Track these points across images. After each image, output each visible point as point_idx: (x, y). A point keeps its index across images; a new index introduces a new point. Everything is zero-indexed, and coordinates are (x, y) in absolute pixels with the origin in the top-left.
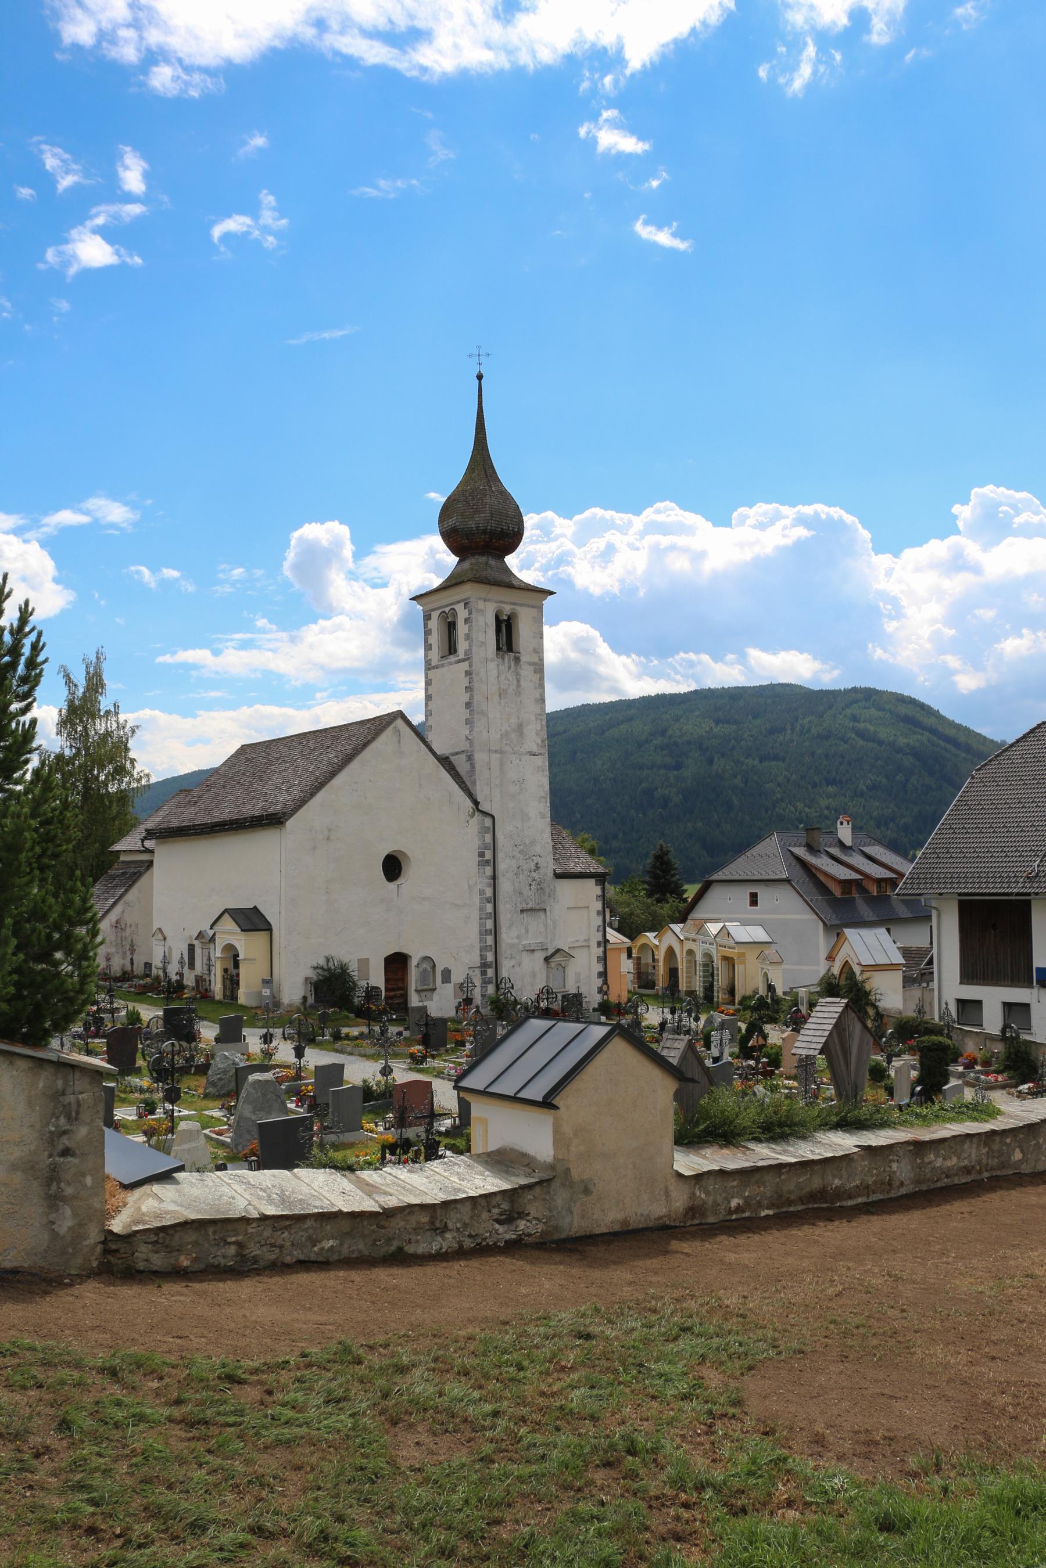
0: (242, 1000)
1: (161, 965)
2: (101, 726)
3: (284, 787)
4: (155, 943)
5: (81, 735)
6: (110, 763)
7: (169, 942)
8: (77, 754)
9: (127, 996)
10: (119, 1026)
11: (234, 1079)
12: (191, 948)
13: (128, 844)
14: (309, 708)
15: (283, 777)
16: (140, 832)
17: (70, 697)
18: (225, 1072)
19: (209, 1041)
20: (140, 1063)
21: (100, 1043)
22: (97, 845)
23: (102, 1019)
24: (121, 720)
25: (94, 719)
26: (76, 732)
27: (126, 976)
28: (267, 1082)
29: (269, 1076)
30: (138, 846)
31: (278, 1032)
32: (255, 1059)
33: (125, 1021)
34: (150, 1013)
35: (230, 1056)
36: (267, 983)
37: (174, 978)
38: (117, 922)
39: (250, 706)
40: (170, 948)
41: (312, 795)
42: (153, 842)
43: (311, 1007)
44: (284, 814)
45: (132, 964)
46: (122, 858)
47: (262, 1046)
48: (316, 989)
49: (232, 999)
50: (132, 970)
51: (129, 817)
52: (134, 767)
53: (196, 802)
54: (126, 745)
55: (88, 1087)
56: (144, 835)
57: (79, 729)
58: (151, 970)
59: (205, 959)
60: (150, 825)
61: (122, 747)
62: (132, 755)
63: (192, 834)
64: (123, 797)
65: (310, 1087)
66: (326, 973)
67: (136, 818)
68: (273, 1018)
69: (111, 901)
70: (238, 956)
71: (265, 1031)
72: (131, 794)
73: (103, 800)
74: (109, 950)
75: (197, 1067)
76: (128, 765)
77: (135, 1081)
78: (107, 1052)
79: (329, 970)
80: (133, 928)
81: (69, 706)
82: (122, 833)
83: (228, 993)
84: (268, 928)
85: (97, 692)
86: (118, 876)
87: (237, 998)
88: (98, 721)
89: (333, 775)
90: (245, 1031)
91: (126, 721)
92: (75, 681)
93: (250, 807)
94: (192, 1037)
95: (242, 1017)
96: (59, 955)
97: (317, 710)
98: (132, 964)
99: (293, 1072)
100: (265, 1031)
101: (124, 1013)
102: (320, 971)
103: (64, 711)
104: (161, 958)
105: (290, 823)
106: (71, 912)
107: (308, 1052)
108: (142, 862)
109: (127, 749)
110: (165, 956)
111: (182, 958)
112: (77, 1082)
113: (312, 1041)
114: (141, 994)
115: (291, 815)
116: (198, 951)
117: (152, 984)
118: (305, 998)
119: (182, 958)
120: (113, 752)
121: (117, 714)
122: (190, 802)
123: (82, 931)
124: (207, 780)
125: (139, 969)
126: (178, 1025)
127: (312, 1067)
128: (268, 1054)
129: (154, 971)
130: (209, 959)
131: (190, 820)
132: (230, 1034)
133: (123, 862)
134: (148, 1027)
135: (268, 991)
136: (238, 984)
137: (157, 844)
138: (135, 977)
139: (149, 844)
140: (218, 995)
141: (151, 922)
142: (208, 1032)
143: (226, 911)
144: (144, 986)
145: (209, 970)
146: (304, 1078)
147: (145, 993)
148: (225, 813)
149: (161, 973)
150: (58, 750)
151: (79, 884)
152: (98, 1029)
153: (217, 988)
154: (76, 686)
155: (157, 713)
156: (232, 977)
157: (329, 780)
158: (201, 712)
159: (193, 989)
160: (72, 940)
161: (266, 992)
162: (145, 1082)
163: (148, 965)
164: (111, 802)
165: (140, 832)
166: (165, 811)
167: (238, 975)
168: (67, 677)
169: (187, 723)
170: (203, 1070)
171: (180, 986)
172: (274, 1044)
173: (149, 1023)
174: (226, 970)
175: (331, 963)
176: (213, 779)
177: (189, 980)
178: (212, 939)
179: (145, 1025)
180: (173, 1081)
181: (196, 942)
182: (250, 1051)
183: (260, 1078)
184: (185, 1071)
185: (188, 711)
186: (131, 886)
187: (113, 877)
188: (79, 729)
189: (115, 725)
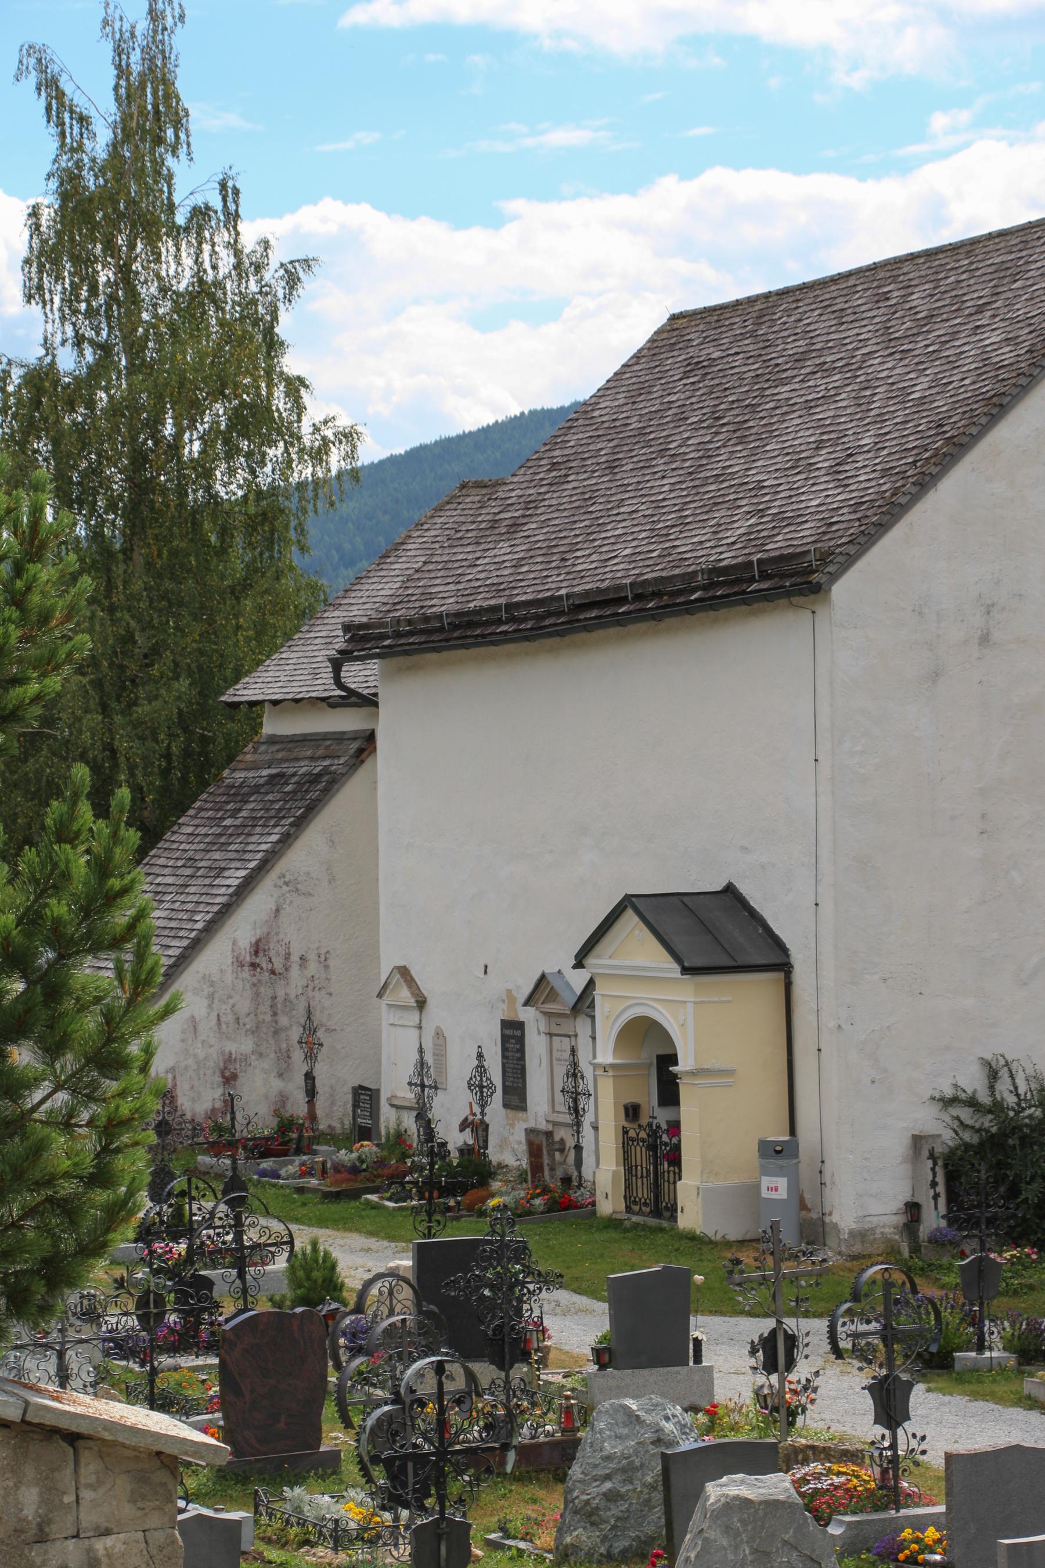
0: (692, 1214)
1: (408, 1096)
2: (178, 266)
3: (823, 460)
4: (387, 1017)
5: (112, 298)
6: (218, 394)
7: (436, 1015)
8: (96, 374)
9: (299, 1204)
10: (263, 1307)
11: (658, 1497)
12: (513, 1034)
13: (288, 675)
14: (904, 168)
15: (820, 424)
16: (325, 636)
17: (65, 162)
18: (629, 1471)
19: (576, 1359)
20: (335, 1437)
21: (195, 1368)
22: (183, 684)
23: (208, 1283)
24: (249, 240)
25: (153, 242)
26: (94, 290)
27: (288, 1138)
28: (772, 1506)
29: (776, 1485)
30: (324, 685)
31: (812, 1330)
32: (734, 1428)
33: (284, 1290)
34: (370, 1261)
35: (646, 1411)
36: (779, 1153)
37: (455, 1139)
38: (257, 948)
39: (688, 174)
40: (439, 1034)
41: (925, 483)
42: (374, 667)
43: (937, 1240)
44: (825, 557)
45: (311, 1092)
46: (271, 726)
47: (761, 1379)
48: (951, 1177)
49: (657, 1213)
50: (312, 1116)
51: (288, 583)
52: (299, 408)
53: (515, 526)
54: (269, 331)
55: (128, 1510)
56: (340, 643)
57: (105, 275)
58: (374, 1113)
59: (561, 1070)
60: (359, 608)
61: (257, 337)
62: (291, 364)
63: (506, 639)
64: (267, 516)
65: (931, 1534)
66: (987, 1121)
67: (314, 588)
68: (794, 1279)
69: (235, 877)
70: (673, 1059)
71: (768, 1324)
72: (293, 504)
73: (196, 525)
74: (231, 1047)
75: (526, 1453)
76: (280, 402)
77: (316, 1502)
78: (223, 1403)
79: (997, 1108)
80: (313, 968)
81: (65, 197)
82: (267, 641)
83: (643, 1192)
84: (776, 961)
85: (159, 141)
86: (256, 789)
87: (673, 1211)
88: (166, 248)
89: (997, 407)
90: (702, 1327)
91: (266, 244)
92: (81, 103)
93: (702, 534)
94: (513, 1344)
95: (687, 1274)
96: (22, 1056)
97: (934, 177)
98: (311, 1092)
99: (869, 1475)
100: (770, 1323)
101: (280, 1263)
102: (965, 1114)
103: (46, 216)
104: (407, 1069)
105: (839, 590)
106: (59, 908)
107: (922, 1399)
108: (339, 737)
109: (273, 345)
110: (422, 1064)
111: (481, 1069)
112: (87, 1495)
113: (938, 1363)
114: (345, 1194)
115: (851, 560)
116: (536, 1045)
117: (381, 1163)
118: (913, 1209)
119: (481, 1069)
120: (224, 355)
121: (232, 218)
122: (494, 524)
123: (96, 972)
124: (553, 443)
125: (334, 1111)
126: (470, 1308)
127: (935, 1459)
128: (781, 1411)
129: (388, 1118)
130: (574, 1073)
131: (497, 589)
132: (649, 1336)
133: (273, 740)
134: (359, 1309)
135: (782, 1183)
136: (675, 1158)
137: (386, 676)
138: (321, 1137)
139: (360, 675)
140: (609, 1203)
141: (374, 946)
142: (571, 1326)
143: (628, 903)
144: (354, 1170)
145: (576, 1111)
146: (912, 1500)
147: (355, 1195)
148: (617, 557)
149: (409, 1122)
150: (33, 354)
151: (85, 810)
152: (192, 1317)
153: (604, 1172)
154: (83, 120)
155: (362, 215)
156: (654, 1133)
157: (985, 429)
158: (518, 205)
159: (522, 1178)
160: (69, 1004)
161: (776, 1187)
162: (352, 1506)
163: (365, 1097)
164: (224, 532)
165: (325, 636)
166: (411, 558)
167: (675, 1128)
168: (51, 87)
169: (469, 248)
170: (550, 1462)
171: (474, 1171)
172: (802, 1371)
173: (362, 1294)
174: (632, 1112)
175: (1003, 1086)
176: (573, 439)
177: (507, 1148)
178: (584, 1003)
179: (352, 1299)
180: (441, 1499)
181: (528, 1016)
182: (721, 1395)
183: (745, 1492)
184: (483, 1462)
185: (471, 206)
186: (301, 823)
187: (241, 795)
188: (105, 275)
189: (226, 261)
